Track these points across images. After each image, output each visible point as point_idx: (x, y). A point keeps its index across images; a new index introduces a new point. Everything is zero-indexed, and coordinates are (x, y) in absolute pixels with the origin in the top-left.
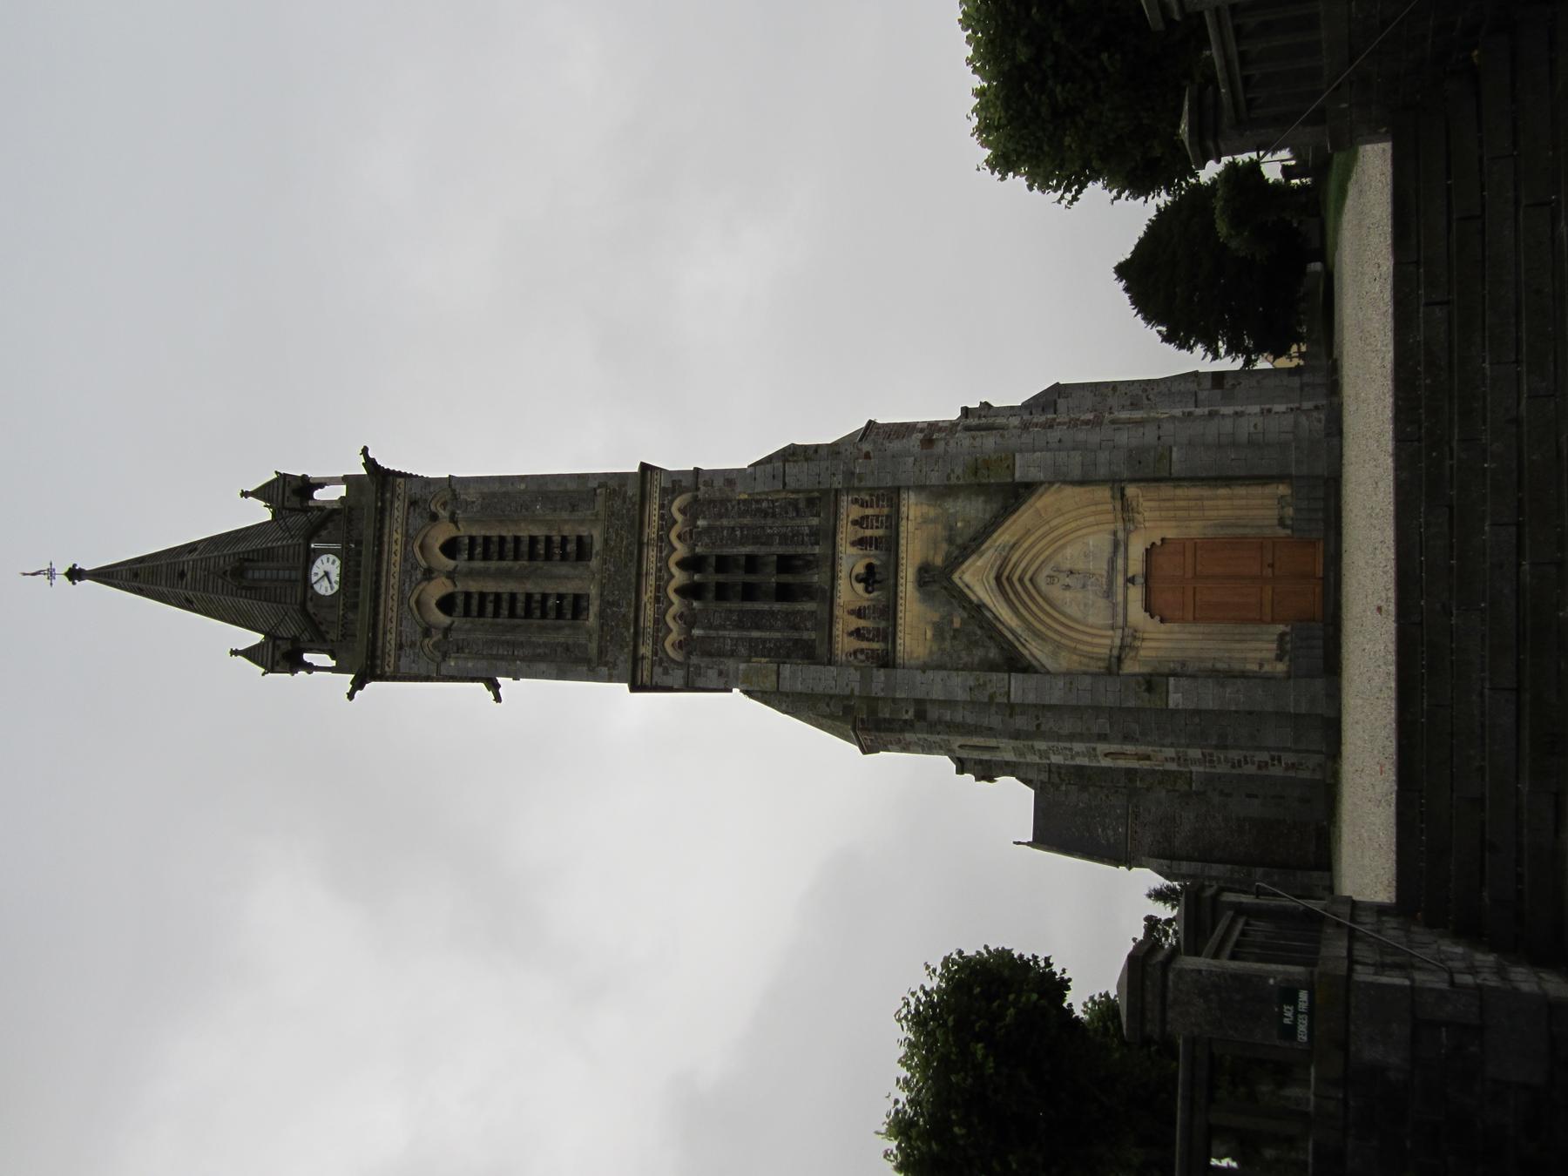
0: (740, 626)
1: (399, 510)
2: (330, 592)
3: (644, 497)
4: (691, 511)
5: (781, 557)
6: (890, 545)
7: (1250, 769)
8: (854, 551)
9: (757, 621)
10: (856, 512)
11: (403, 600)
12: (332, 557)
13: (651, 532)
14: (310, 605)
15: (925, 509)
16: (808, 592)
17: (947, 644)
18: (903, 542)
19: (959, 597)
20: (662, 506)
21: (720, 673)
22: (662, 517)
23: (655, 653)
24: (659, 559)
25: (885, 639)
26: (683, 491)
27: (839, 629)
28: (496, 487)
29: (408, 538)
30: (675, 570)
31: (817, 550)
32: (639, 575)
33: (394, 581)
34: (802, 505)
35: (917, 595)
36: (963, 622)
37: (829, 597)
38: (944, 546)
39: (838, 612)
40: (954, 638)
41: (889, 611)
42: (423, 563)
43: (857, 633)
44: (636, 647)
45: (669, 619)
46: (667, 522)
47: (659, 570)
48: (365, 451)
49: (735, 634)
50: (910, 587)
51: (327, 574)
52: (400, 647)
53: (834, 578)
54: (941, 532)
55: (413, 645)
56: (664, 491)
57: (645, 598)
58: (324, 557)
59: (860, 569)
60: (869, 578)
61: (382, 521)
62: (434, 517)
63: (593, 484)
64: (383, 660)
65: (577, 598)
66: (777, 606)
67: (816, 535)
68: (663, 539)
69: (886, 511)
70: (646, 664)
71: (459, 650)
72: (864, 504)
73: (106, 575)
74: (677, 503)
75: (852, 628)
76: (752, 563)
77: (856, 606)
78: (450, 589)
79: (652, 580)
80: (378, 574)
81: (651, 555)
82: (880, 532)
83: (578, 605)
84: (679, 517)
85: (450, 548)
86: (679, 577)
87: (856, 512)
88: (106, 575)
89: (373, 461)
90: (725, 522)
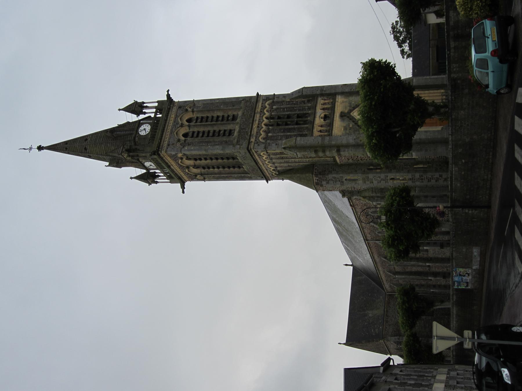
0: (284, 132)
1: (174, 109)
2: (145, 134)
3: (257, 101)
4: (271, 105)
5: (298, 114)
6: (333, 109)
7: (433, 182)
8: (320, 111)
9: (289, 130)
10: (322, 102)
11: (172, 132)
12: (147, 125)
13: (258, 110)
14: (137, 138)
15: (343, 99)
16: (305, 122)
17: (348, 132)
18: (336, 107)
19: (352, 119)
20: (262, 104)
21: (276, 144)
22: (262, 106)
23: (256, 140)
24: (260, 117)
25: (329, 132)
26: (269, 99)
27: (315, 130)
28: (209, 102)
29: (176, 116)
30: (263, 126)
31: (310, 112)
32: (253, 121)
33: (170, 128)
34: (306, 102)
35: (339, 120)
36: (353, 125)
37: (313, 123)
38: (348, 108)
39: (315, 126)
40: (350, 129)
41: (331, 125)
42: (180, 122)
43: (320, 131)
44: (250, 139)
45: (261, 132)
46: (264, 107)
47: (260, 119)
48: (168, 91)
49: (282, 134)
50: (337, 118)
51: (145, 129)
52: (169, 145)
53: (315, 117)
54: (347, 104)
55: (173, 144)
56: (263, 100)
57: (254, 127)
58: (145, 125)
59: (323, 115)
60: (325, 117)
61: (169, 111)
62: (187, 110)
63: (240, 99)
64: (162, 149)
65: (230, 130)
66: (296, 126)
67: (309, 108)
68: (262, 112)
69: (331, 101)
70: (253, 144)
71: (189, 145)
72: (325, 100)
73: (54, 148)
74: (267, 102)
75: (322, 108)
76: (289, 117)
77: (320, 124)
78: (188, 131)
79: (257, 122)
80: (165, 125)
81: (257, 116)
82: (329, 106)
83: (231, 133)
84: (268, 106)
85: (189, 121)
86: (266, 121)
87: (322, 102)
88: (54, 148)
89: (170, 95)
90: (282, 107)
